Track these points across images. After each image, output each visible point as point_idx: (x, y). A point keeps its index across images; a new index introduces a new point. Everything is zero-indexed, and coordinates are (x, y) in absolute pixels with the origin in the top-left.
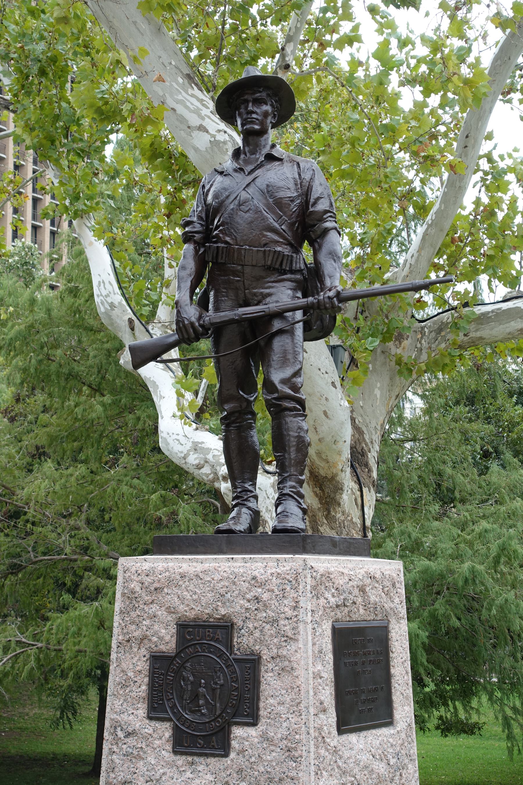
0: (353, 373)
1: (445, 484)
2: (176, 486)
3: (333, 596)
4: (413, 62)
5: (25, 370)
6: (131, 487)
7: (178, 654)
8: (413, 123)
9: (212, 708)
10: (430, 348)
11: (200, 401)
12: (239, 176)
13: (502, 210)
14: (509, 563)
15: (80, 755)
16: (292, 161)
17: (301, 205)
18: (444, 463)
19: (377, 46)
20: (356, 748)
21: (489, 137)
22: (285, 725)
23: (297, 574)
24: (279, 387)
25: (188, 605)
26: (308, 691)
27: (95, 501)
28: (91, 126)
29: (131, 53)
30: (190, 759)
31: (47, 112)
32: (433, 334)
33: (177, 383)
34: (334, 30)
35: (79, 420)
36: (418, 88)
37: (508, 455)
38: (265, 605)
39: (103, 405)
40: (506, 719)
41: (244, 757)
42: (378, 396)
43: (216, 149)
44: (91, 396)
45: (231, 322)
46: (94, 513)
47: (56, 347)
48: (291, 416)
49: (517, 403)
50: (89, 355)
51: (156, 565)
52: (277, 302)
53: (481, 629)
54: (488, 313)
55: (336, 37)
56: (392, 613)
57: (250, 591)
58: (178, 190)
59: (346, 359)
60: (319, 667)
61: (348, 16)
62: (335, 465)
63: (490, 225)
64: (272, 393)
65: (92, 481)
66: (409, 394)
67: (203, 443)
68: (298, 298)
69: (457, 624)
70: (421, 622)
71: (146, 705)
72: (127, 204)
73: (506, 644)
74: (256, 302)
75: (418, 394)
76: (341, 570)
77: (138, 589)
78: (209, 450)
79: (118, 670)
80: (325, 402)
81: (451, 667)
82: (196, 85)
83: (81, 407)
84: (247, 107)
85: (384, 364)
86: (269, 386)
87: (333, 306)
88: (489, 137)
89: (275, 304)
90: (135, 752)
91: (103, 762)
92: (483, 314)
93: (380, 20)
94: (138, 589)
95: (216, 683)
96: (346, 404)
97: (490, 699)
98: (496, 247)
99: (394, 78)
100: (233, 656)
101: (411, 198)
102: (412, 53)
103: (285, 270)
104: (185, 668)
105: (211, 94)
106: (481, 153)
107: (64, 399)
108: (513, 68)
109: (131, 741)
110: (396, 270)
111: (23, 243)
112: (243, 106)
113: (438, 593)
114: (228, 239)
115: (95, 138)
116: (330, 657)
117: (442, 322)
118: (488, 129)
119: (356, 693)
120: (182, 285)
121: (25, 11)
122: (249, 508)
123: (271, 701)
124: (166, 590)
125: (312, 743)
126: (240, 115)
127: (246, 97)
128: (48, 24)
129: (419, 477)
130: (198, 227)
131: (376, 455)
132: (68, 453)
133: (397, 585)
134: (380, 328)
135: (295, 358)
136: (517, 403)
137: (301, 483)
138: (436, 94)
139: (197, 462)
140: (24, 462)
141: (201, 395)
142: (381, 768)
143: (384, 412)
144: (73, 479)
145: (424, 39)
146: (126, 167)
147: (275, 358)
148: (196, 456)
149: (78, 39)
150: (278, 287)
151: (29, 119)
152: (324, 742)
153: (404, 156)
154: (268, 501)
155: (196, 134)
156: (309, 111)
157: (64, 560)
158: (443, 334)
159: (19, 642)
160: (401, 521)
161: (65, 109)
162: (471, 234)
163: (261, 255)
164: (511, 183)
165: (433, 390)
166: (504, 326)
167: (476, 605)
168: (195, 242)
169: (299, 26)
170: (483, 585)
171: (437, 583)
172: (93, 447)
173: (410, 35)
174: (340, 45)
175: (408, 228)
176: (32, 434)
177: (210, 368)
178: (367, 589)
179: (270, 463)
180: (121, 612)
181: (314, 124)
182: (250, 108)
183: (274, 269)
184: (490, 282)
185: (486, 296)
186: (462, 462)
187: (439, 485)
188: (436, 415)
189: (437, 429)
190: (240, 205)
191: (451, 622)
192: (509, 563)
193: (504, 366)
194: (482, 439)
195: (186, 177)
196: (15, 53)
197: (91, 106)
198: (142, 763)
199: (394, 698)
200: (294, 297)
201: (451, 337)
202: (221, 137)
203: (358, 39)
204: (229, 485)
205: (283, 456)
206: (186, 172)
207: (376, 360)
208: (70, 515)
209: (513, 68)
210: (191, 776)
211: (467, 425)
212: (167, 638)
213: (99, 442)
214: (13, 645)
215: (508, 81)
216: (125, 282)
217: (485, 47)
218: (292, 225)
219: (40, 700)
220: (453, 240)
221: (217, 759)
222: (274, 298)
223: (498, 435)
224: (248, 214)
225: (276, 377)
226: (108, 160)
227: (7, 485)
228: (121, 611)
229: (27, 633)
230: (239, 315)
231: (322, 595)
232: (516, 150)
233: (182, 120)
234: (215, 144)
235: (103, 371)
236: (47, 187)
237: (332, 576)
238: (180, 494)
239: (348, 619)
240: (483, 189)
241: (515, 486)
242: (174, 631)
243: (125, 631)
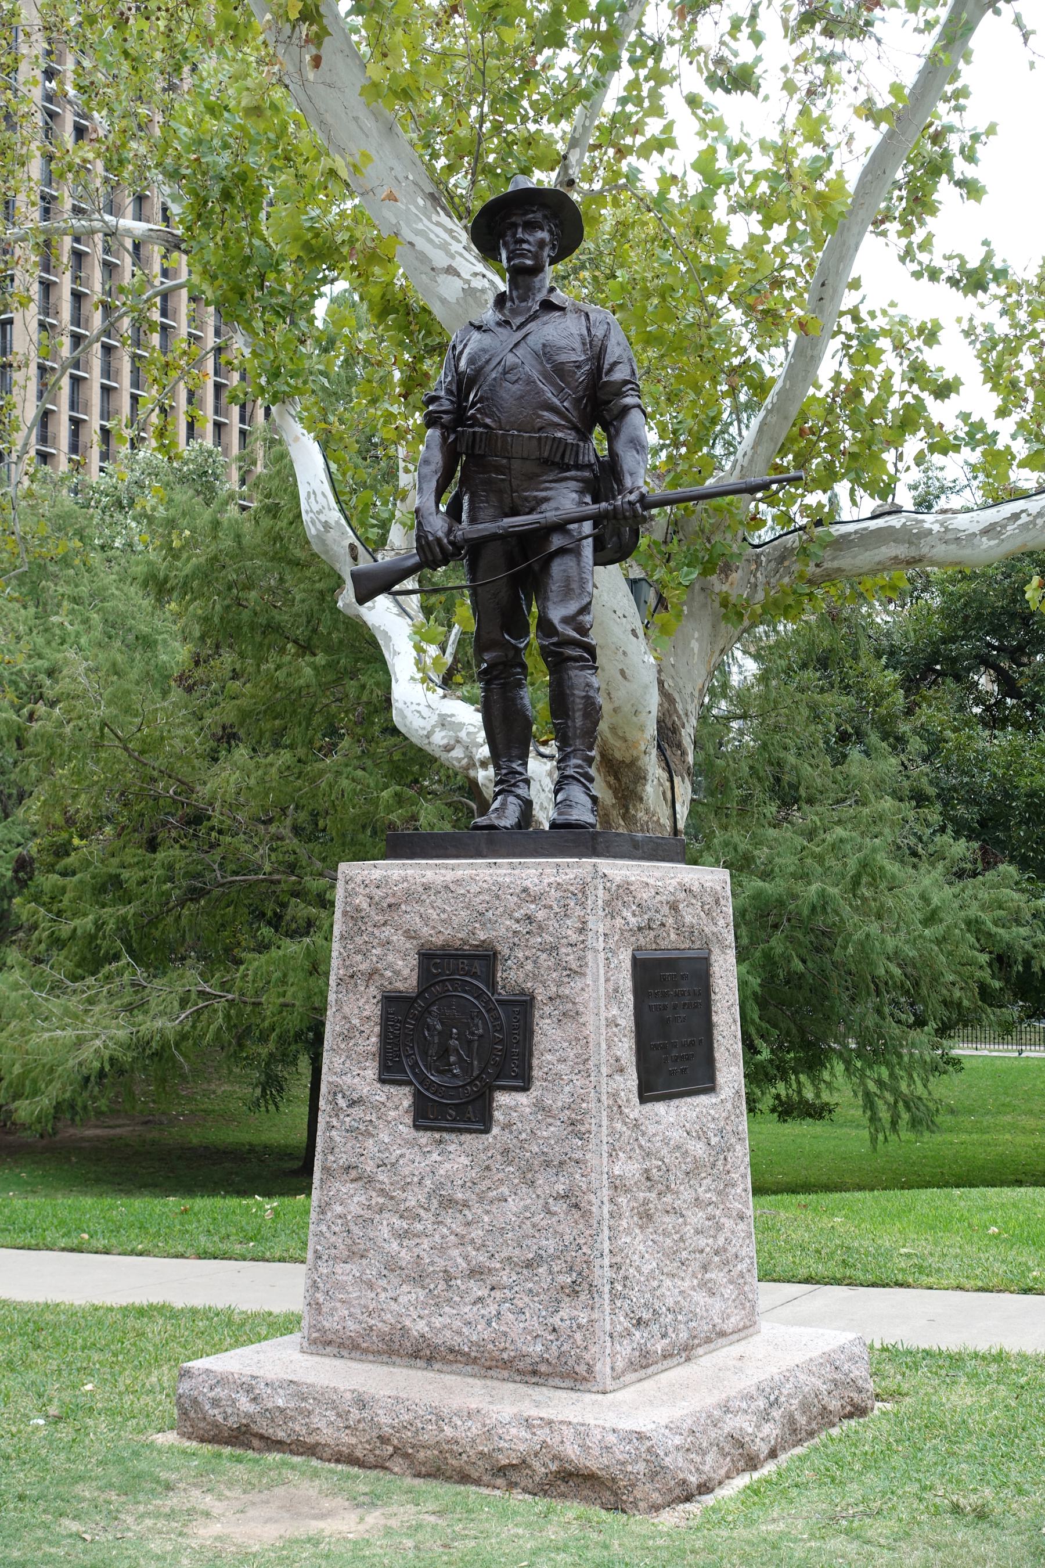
0: (662, 617)
1: (786, 778)
2: (416, 781)
3: (634, 915)
4: (748, 179)
5: (206, 620)
6: (353, 780)
7: (420, 994)
8: (749, 264)
9: (466, 1068)
10: (768, 583)
11: (448, 659)
12: (503, 333)
13: (872, 390)
14: (873, 884)
15: (286, 1146)
16: (578, 311)
17: (590, 372)
18: (785, 748)
19: (697, 155)
20: (664, 1121)
21: (855, 284)
22: (567, 1089)
23: (585, 884)
24: (560, 627)
25: (434, 928)
26: (599, 1044)
27: (303, 802)
28: (295, 274)
29: (349, 159)
30: (437, 1136)
31: (233, 252)
32: (773, 564)
33: (415, 633)
34: (636, 131)
35: (280, 689)
36: (756, 216)
37: (874, 738)
38: (540, 927)
39: (315, 668)
40: (867, 1094)
41: (511, 1132)
42: (696, 651)
43: (470, 299)
44: (297, 655)
45: (493, 537)
46: (303, 816)
47: (248, 587)
48: (577, 668)
49: (886, 667)
50: (294, 598)
51: (389, 873)
52: (557, 509)
53: (834, 974)
54: (850, 534)
55: (639, 140)
56: (714, 939)
57: (520, 907)
58: (418, 359)
59: (652, 598)
60: (615, 1011)
61: (657, 111)
62: (635, 745)
63: (853, 411)
64: (549, 636)
65: (300, 773)
66: (738, 654)
67: (453, 715)
68: (587, 504)
69: (801, 967)
70: (752, 965)
71: (376, 1064)
72: (346, 387)
73: (869, 994)
75: (750, 654)
76: (645, 879)
77: (365, 905)
78: (461, 725)
79: (339, 1016)
80: (622, 657)
81: (792, 1026)
82: (443, 208)
83: (284, 671)
84: (514, 234)
85: (705, 605)
86: (546, 626)
87: (635, 514)
88: (855, 284)
89: (554, 513)
90: (362, 1127)
91: (318, 1140)
92: (842, 536)
93: (703, 115)
94: (365, 905)
95: (473, 1034)
96: (652, 660)
97: (847, 1069)
98: (861, 442)
99: (721, 200)
100: (496, 996)
101: (744, 373)
102: (748, 167)
103: (568, 465)
104: (430, 1013)
105: (464, 221)
106: (843, 308)
107: (260, 660)
108: (888, 186)
109: (357, 1112)
110: (722, 474)
111: (201, 445)
112: (509, 233)
113: (776, 926)
114: (488, 421)
115: (300, 289)
116: (629, 998)
117: (785, 548)
118: (854, 274)
119: (664, 1047)
120: (425, 486)
121: (202, 108)
122: (518, 796)
123: (549, 1057)
124: (403, 907)
125: (605, 1113)
126: (505, 245)
127: (513, 219)
128: (234, 126)
129: (751, 768)
130: (446, 405)
131: (692, 732)
132: (267, 734)
133: (722, 902)
134: (700, 555)
135: (582, 588)
136: (886, 667)
137: (590, 761)
138: (781, 224)
139: (445, 742)
140: (207, 747)
141: (450, 650)
142: (698, 1149)
143: (704, 673)
144: (274, 770)
145: (765, 146)
146: (346, 331)
147: (554, 588)
148: (443, 733)
149: (276, 147)
151: (208, 262)
152: (621, 1113)
153: (735, 315)
154: (543, 795)
155: (442, 278)
156: (601, 253)
157: (263, 881)
158: (786, 563)
159: (201, 993)
160: (725, 828)
161: (258, 248)
162: (827, 423)
163: (535, 443)
164: (884, 351)
165: (770, 647)
166: (872, 553)
167: (828, 943)
168: (443, 426)
169: (587, 124)
170: (838, 915)
171: (774, 911)
172: (300, 725)
173: (745, 140)
174: (645, 152)
175: (740, 421)
176: (216, 709)
177: (464, 609)
178: (681, 906)
179: (545, 743)
180: (342, 937)
181: (608, 271)
182: (520, 235)
183: (553, 463)
184: (852, 491)
185: (847, 512)
186: (810, 748)
187: (778, 780)
188: (774, 683)
189: (775, 702)
190: (505, 372)
191: (793, 965)
192: (873, 884)
193: (870, 615)
194: (838, 715)
195: (428, 341)
196: (187, 167)
197: (296, 238)
198: (371, 1141)
199: (717, 1055)
200: (581, 503)
201: (796, 567)
202: (478, 283)
203: (671, 143)
204: (491, 770)
205: (566, 723)
206: (429, 333)
207: (693, 599)
208: (270, 821)
209: (888, 186)
210: (439, 1158)
211: (817, 697)
212: (406, 972)
213: (309, 721)
214: (193, 996)
215: (883, 205)
216: (344, 494)
217: (850, 157)
218: (577, 401)
219: (230, 1072)
220: (802, 432)
221: (474, 1135)
222: (552, 504)
223: (860, 710)
224: (517, 386)
225: (556, 614)
226: (319, 323)
227: (184, 779)
228: (342, 936)
229: (213, 981)
230: (504, 528)
231: (619, 913)
232: (893, 304)
233: (423, 258)
234: (470, 292)
235: (315, 622)
236: (236, 361)
237: (632, 888)
238: (423, 792)
239: (654, 946)
240: (846, 359)
241: (883, 781)
242: (415, 962)
243: (347, 963)
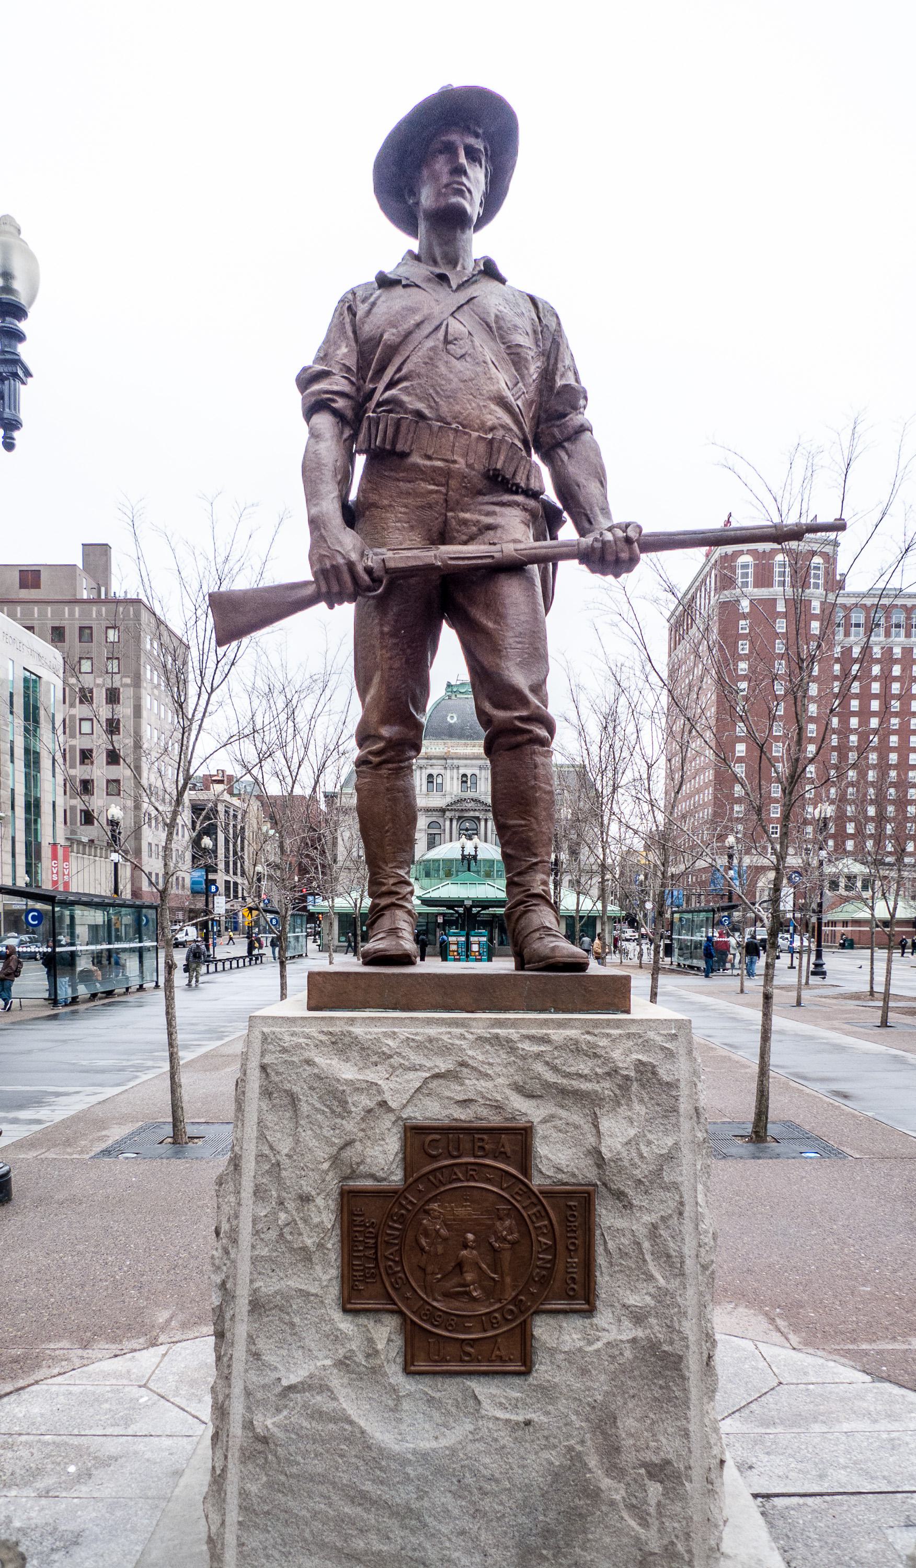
74: (464, 538)
103: (518, 486)
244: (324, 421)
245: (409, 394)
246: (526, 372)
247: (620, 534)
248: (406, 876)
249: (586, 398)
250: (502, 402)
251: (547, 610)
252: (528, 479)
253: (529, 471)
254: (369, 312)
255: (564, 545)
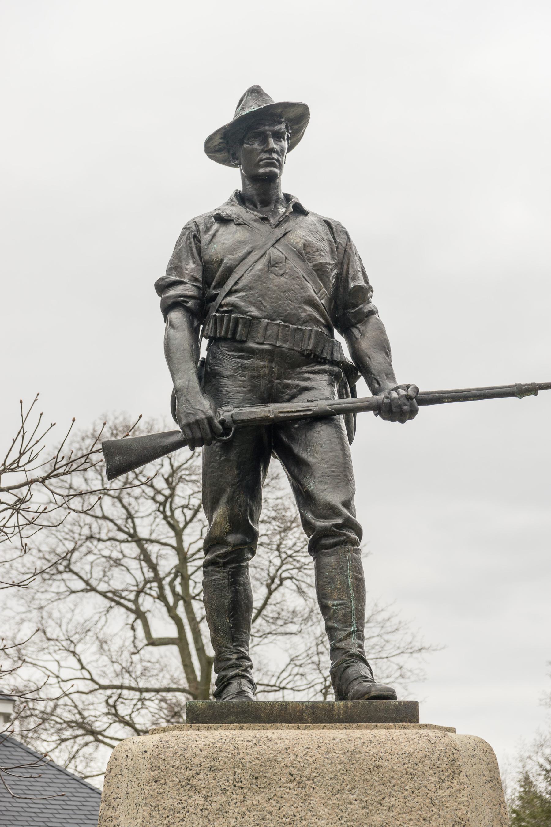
103: (325, 359)
150: (317, 380)
244: (176, 316)
245: (244, 301)
246: (327, 280)
247: (402, 392)
248: (247, 653)
249: (372, 291)
250: (311, 302)
251: (351, 440)
252: (332, 353)
253: (333, 348)
254: (211, 241)
255: (363, 400)
